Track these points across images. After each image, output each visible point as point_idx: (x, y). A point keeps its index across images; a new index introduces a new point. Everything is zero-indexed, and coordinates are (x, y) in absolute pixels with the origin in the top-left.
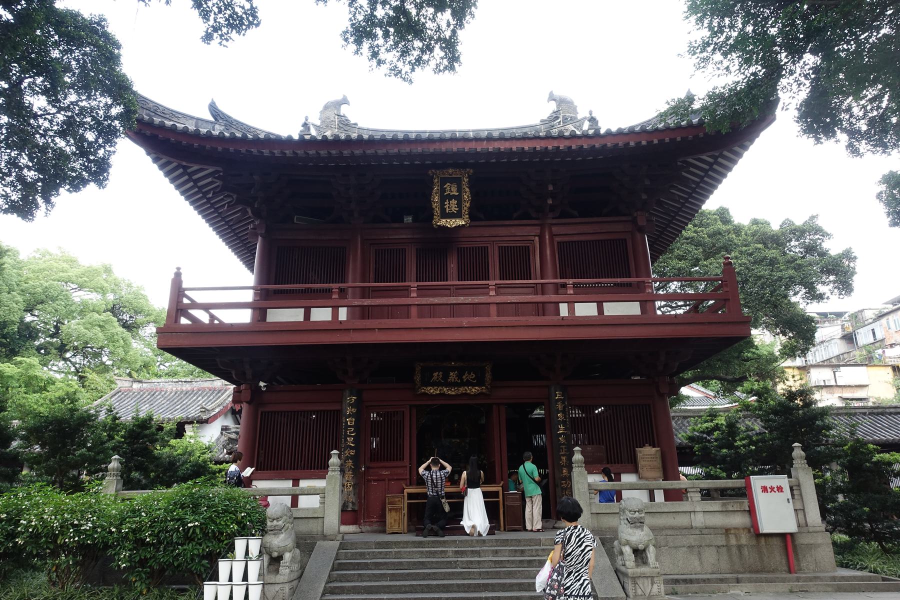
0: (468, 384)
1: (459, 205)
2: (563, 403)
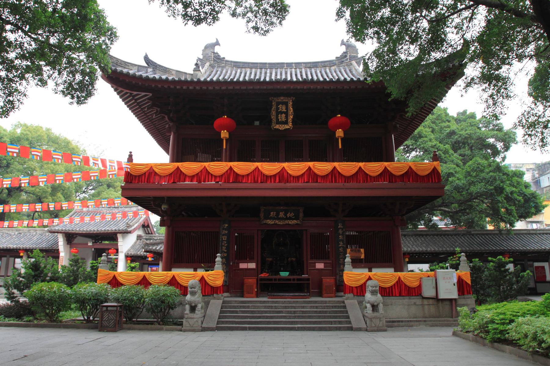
0: (290, 218)
2: (342, 230)
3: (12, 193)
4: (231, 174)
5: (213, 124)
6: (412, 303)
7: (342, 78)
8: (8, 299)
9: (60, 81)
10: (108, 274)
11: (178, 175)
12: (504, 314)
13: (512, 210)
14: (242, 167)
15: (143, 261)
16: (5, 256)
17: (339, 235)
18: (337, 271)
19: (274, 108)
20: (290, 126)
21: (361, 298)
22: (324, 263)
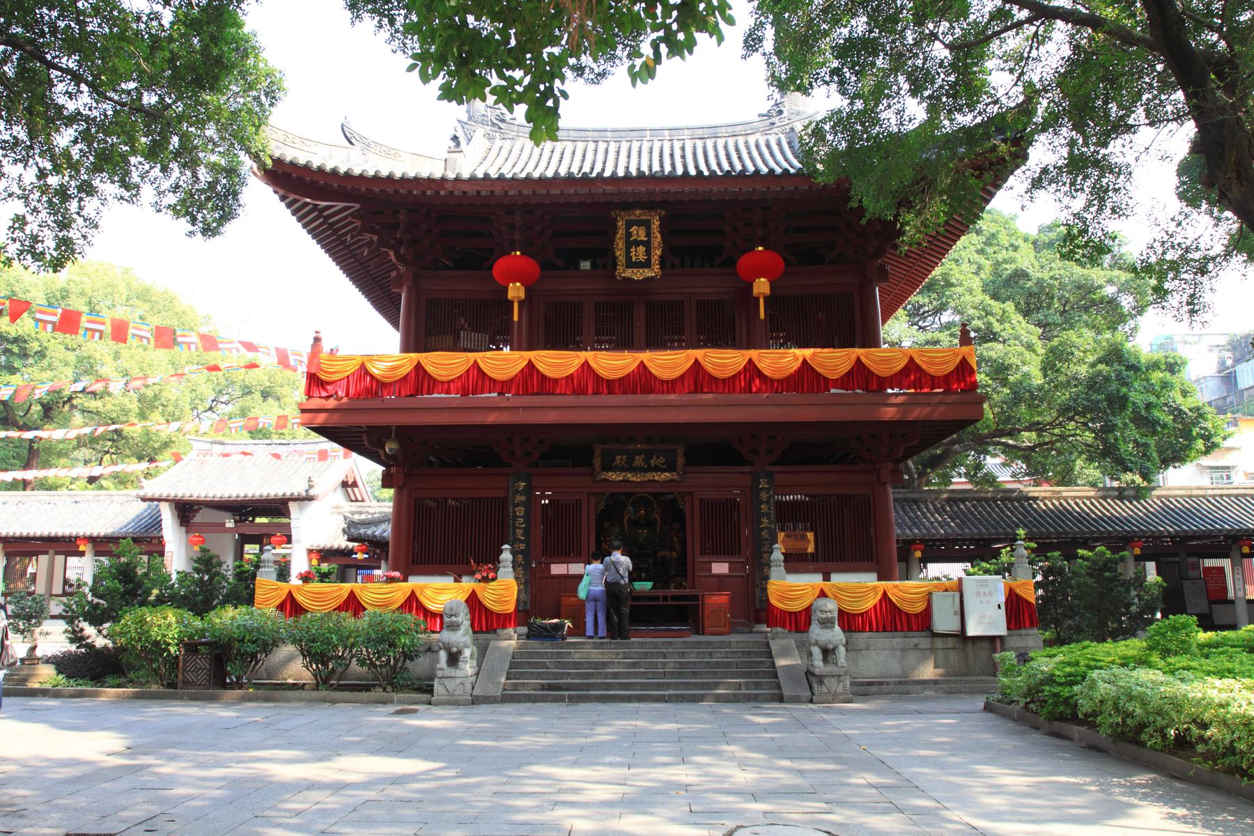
0: (657, 469)
1: (648, 252)
3: (54, 413)
4: (531, 380)
5: (490, 268)
6: (912, 645)
7: (765, 170)
8: (72, 641)
9: (166, 185)
10: (276, 590)
11: (420, 380)
12: (1077, 664)
13: (1146, 445)
14: (556, 363)
15: (345, 561)
16: (46, 553)
17: (762, 502)
18: (757, 581)
19: (621, 233)
20: (654, 272)
21: (803, 636)
22: (730, 563)
